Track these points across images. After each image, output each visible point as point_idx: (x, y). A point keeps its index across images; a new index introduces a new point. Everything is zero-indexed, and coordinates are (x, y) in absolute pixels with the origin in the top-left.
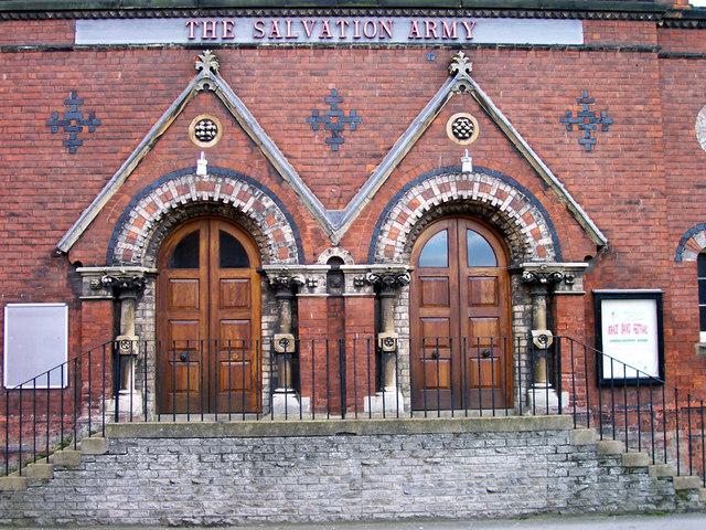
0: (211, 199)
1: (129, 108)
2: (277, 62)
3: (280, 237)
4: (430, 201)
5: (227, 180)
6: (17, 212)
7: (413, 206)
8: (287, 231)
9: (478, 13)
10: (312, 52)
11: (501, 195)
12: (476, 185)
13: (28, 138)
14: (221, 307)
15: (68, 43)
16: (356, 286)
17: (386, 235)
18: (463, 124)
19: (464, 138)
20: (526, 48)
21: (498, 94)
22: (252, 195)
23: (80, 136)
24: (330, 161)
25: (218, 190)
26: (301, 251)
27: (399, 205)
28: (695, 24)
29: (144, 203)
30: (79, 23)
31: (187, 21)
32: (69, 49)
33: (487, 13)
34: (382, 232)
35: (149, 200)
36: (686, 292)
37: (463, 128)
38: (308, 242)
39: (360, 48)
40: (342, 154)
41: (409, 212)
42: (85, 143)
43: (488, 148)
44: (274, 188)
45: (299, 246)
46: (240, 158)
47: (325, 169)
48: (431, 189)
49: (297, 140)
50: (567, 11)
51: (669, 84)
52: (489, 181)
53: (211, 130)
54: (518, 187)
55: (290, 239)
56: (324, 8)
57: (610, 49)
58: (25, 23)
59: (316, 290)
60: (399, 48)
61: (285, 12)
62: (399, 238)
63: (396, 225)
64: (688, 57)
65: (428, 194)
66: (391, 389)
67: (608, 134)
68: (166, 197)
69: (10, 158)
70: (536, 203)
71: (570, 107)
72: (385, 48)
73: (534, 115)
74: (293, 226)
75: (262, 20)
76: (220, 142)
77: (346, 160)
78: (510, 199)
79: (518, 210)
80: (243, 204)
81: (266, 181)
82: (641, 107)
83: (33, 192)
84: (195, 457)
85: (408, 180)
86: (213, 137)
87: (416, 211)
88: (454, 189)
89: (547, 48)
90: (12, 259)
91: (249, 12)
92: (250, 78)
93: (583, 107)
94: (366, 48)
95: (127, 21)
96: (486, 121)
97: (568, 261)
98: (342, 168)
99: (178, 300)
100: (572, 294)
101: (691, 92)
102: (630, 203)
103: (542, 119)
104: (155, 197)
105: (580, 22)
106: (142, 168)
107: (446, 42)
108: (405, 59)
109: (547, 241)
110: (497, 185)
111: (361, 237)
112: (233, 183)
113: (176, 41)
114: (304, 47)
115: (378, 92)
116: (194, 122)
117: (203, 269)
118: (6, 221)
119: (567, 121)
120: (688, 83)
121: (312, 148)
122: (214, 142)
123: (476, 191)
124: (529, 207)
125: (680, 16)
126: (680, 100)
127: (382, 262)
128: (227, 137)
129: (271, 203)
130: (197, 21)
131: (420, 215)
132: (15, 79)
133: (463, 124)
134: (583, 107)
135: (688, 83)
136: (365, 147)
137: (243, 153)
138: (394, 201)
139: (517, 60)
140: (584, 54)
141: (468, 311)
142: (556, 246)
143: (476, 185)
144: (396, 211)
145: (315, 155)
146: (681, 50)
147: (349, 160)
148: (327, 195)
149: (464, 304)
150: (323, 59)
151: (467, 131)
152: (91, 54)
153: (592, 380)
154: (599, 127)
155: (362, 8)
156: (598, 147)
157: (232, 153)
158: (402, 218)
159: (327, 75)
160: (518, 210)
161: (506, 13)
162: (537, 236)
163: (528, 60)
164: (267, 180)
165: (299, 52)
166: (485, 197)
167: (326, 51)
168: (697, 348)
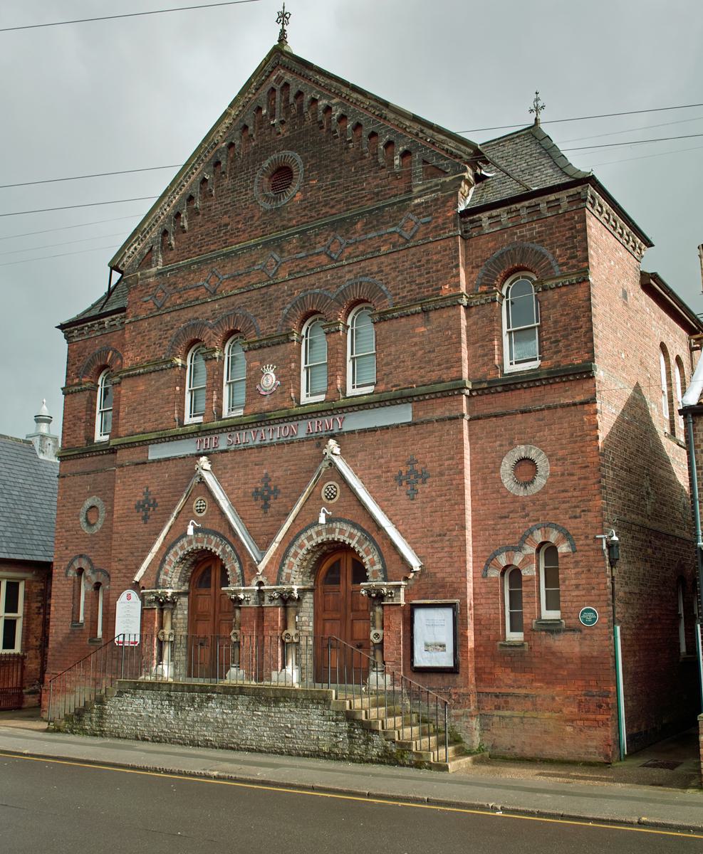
0: (333, 539)
1: (170, 495)
2: (238, 459)
3: (234, 570)
4: (311, 543)
5: (210, 535)
6: (122, 558)
7: (301, 547)
8: (237, 565)
9: (345, 410)
10: (256, 450)
11: (351, 536)
12: (337, 530)
13: (127, 516)
14: (220, 612)
15: (144, 459)
16: (270, 600)
17: (286, 566)
18: (330, 489)
19: (331, 499)
20: (374, 430)
21: (356, 465)
22: (221, 544)
23: (149, 513)
24: (263, 520)
25: (205, 542)
26: (243, 579)
27: (294, 547)
28: (499, 389)
29: (172, 552)
30: (150, 446)
31: (195, 439)
32: (145, 463)
33: (350, 409)
34: (284, 565)
35: (174, 549)
36: (490, 601)
37: (330, 492)
38: (247, 573)
39: (280, 444)
40: (270, 514)
41: (299, 551)
42: (151, 517)
43: (345, 504)
44: (231, 539)
45: (243, 575)
46: (215, 524)
47: (260, 525)
48: (311, 535)
49: (247, 508)
50: (399, 399)
51: (481, 439)
52: (345, 527)
53: (203, 506)
54: (362, 530)
55: (238, 571)
56: (261, 422)
57: (429, 422)
58: (128, 450)
59: (250, 602)
60: (301, 441)
61: (242, 427)
62: (294, 568)
63: (292, 559)
64: (496, 416)
65: (310, 538)
66: (289, 669)
67: (426, 485)
68: (182, 548)
69: (120, 528)
70: (372, 540)
71: (402, 469)
72: (293, 442)
73: (379, 477)
74: (240, 563)
75: (232, 434)
76: (207, 513)
77: (271, 519)
78: (357, 538)
79: (361, 546)
80: (333, 536)
81: (228, 535)
82: (450, 462)
83: (128, 547)
84: (150, 701)
85: (300, 530)
86: (204, 510)
87: (303, 550)
88: (324, 534)
89: (387, 428)
90: (119, 586)
91: (225, 430)
92: (226, 471)
93: (410, 468)
94: (283, 444)
95: (170, 443)
96: (344, 486)
97: (392, 581)
98: (270, 523)
99: (200, 608)
100: (394, 605)
101: (498, 443)
102: (440, 535)
103: (383, 479)
104: (176, 548)
105: (410, 404)
106: (172, 531)
107: (327, 433)
108: (304, 448)
109: (378, 567)
110: (348, 529)
111: (274, 569)
112: (212, 537)
113: (192, 453)
114: (251, 448)
115: (289, 472)
116: (195, 502)
117: (212, 588)
118: (117, 564)
119: (399, 479)
120: (496, 436)
121: (253, 512)
122: (204, 513)
123: (337, 534)
124: (368, 543)
125: (485, 385)
126: (489, 450)
127: (284, 584)
128: (210, 509)
129: (230, 548)
130: (273, 427)
131: (305, 552)
132: (123, 482)
133: (330, 489)
134: (410, 468)
135: (496, 436)
136: (281, 509)
137: (217, 519)
138: (291, 545)
139: (370, 439)
140: (412, 428)
141: (351, 615)
142: (384, 570)
143: (337, 530)
144: (292, 550)
145: (255, 516)
146: (492, 411)
147: (273, 518)
148: (261, 541)
149: (349, 611)
150: (261, 454)
151: (332, 494)
152: (155, 464)
153: (408, 668)
154: (420, 480)
155: (279, 418)
156: (420, 496)
157: (212, 519)
158: (296, 555)
159: (262, 464)
160: (361, 546)
161: (361, 407)
162: (373, 564)
163: (376, 438)
164: (228, 535)
165: (250, 451)
166: (342, 538)
167: (263, 449)
168: (498, 646)
